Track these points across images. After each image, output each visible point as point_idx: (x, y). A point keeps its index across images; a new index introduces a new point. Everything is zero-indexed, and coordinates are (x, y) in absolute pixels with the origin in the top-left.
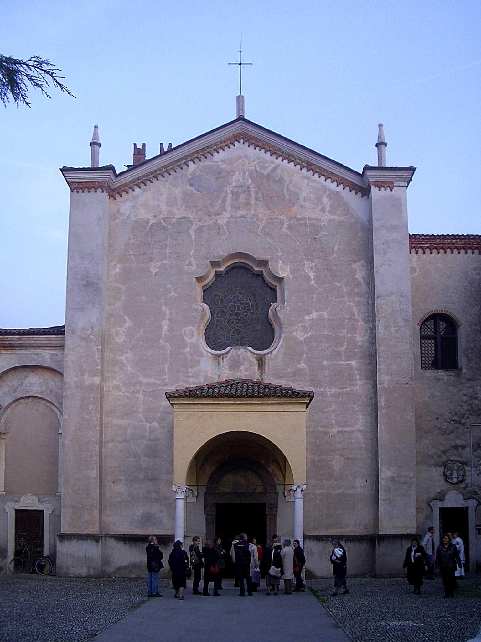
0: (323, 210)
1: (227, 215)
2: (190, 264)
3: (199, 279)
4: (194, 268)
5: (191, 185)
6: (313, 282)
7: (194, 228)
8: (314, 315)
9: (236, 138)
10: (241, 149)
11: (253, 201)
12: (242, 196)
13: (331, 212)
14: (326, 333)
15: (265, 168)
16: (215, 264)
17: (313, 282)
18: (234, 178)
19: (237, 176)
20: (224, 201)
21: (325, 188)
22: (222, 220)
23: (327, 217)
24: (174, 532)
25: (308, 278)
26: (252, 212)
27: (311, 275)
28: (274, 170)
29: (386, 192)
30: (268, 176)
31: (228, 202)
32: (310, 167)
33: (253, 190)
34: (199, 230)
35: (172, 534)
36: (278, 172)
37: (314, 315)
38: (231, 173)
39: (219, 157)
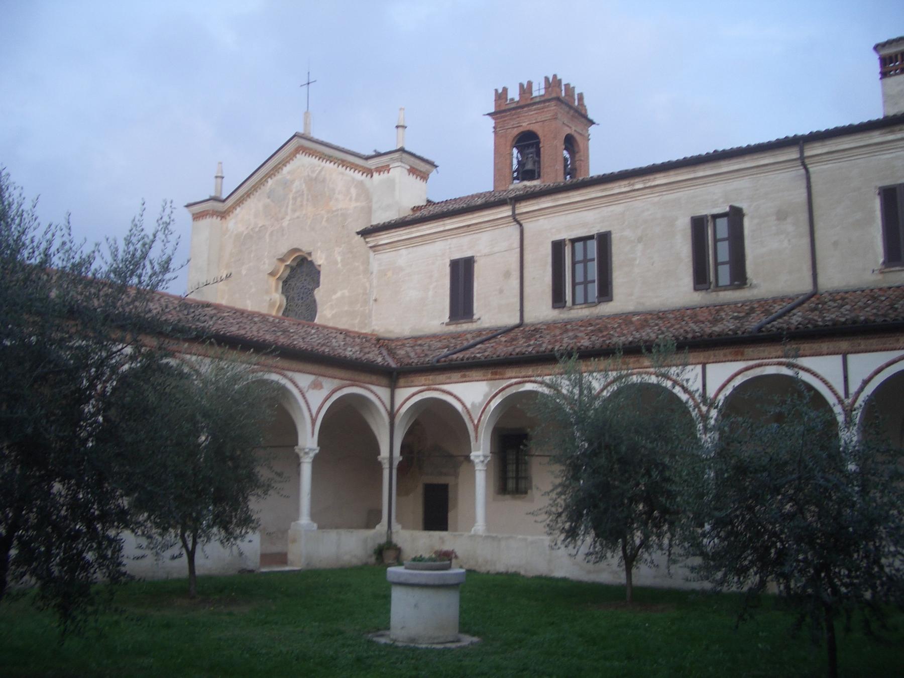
0: (350, 200)
1: (288, 218)
2: (264, 263)
3: (272, 274)
4: (266, 266)
5: (269, 197)
6: (340, 265)
7: (269, 232)
8: (339, 294)
9: (297, 151)
10: (302, 160)
11: (305, 203)
12: (299, 200)
13: (357, 200)
14: (346, 308)
15: (313, 172)
16: (282, 260)
17: (340, 265)
18: (295, 185)
19: (297, 183)
20: (287, 207)
21: (353, 179)
22: (285, 223)
23: (354, 204)
24: (883, 85)
25: (336, 263)
26: (304, 212)
27: (339, 259)
28: (320, 172)
29: (384, 176)
30: (316, 179)
31: (290, 207)
32: (343, 163)
33: (305, 192)
34: (271, 234)
35: (890, 81)
36: (323, 173)
37: (339, 294)
38: (292, 182)
39: (286, 169)
